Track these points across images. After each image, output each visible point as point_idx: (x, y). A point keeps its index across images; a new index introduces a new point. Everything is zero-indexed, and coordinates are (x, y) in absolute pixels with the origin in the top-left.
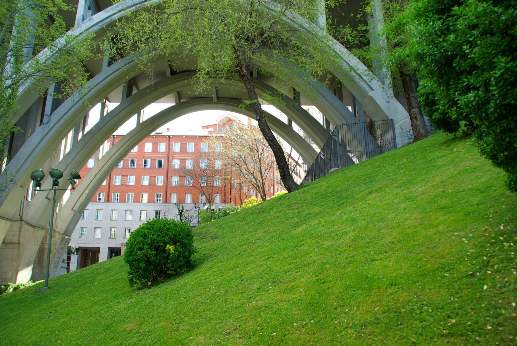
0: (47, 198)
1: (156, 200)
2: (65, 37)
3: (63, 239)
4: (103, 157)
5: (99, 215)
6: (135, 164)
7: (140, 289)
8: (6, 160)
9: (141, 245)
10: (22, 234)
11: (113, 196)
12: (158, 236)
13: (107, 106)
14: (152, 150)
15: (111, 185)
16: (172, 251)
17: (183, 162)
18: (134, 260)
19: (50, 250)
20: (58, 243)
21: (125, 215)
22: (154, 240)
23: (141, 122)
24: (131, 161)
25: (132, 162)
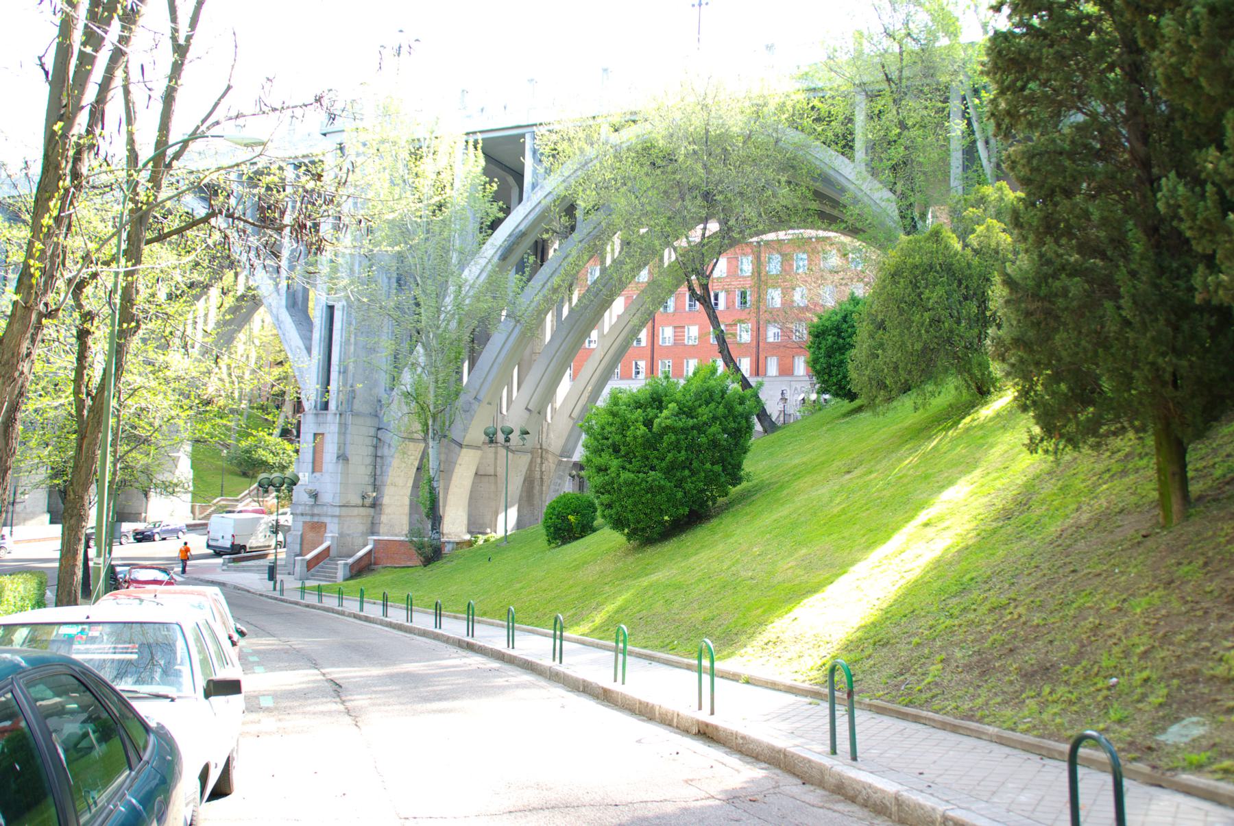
0: (527, 408)
8: (466, 365)
14: (729, 271)
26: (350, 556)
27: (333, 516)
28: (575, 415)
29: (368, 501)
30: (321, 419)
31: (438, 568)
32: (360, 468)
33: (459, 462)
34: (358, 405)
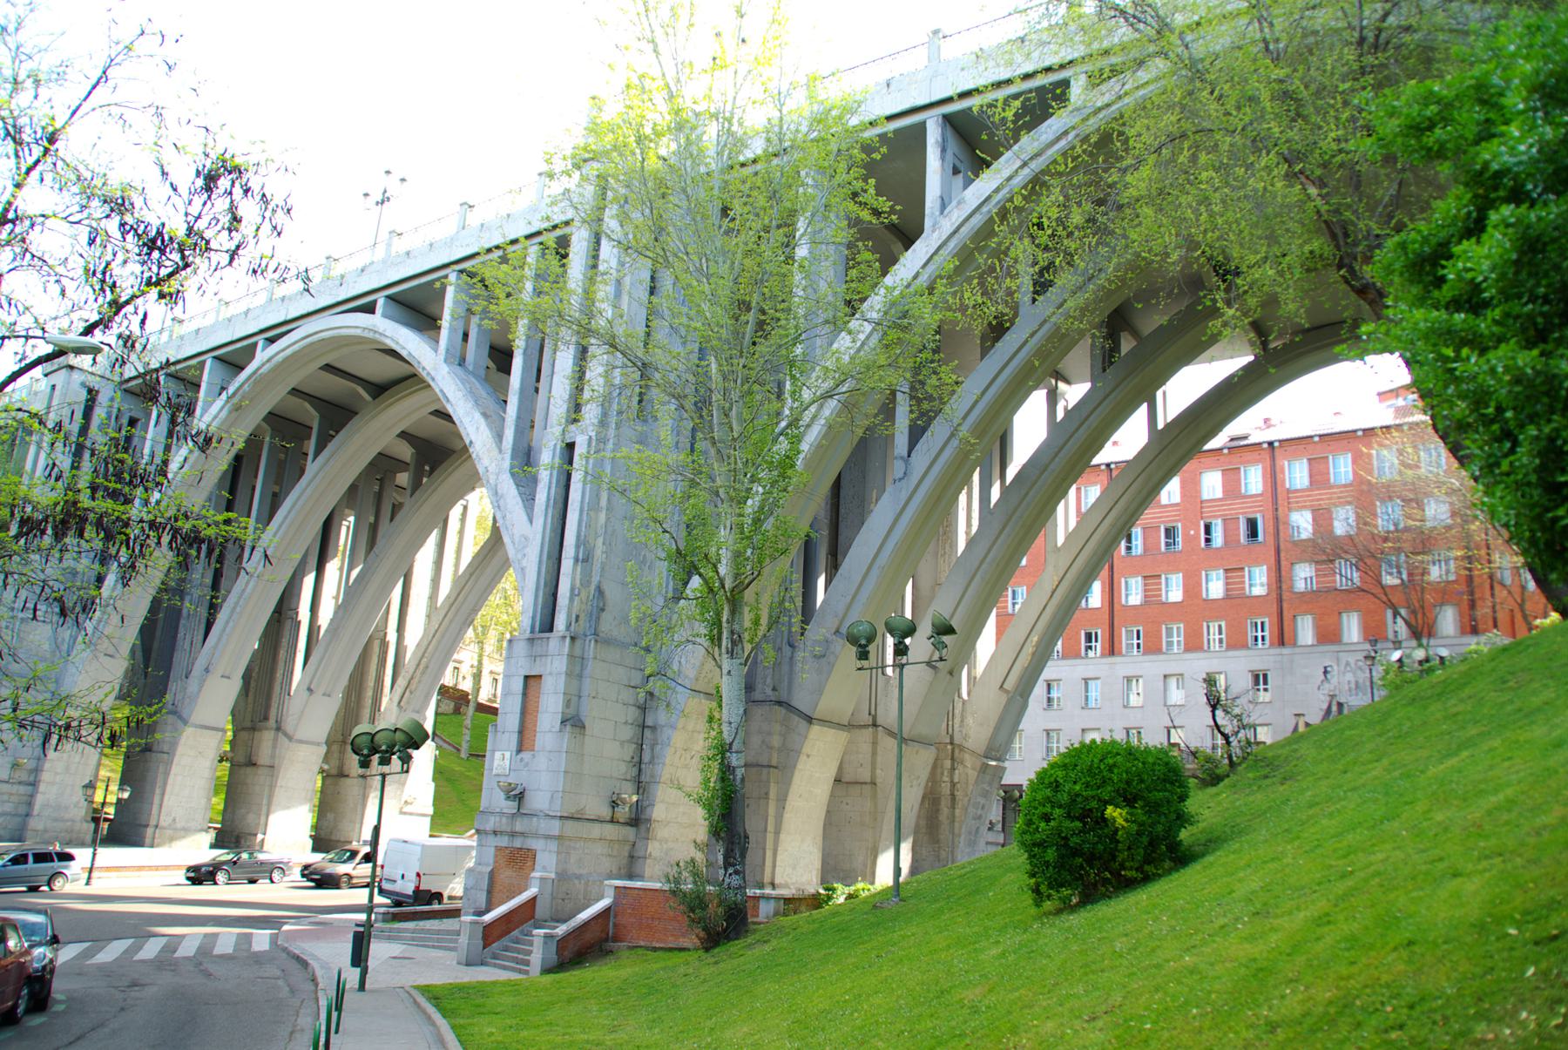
1: (1250, 641)
2: (882, 291)
4: (1069, 537)
5: (1093, 694)
6: (1179, 539)
7: (1059, 912)
9: (1048, 809)
10: (879, 759)
11: (1125, 638)
12: (1087, 785)
13: (1063, 395)
15: (1116, 606)
16: (1120, 821)
17: (1322, 518)
18: (1034, 845)
20: (972, 780)
21: (1165, 690)
22: (1077, 795)
23: (1160, 426)
24: (1167, 530)
25: (1170, 533)
27: (548, 837)
29: (623, 812)
30: (538, 649)
31: (739, 956)
32: (609, 745)
34: (608, 624)
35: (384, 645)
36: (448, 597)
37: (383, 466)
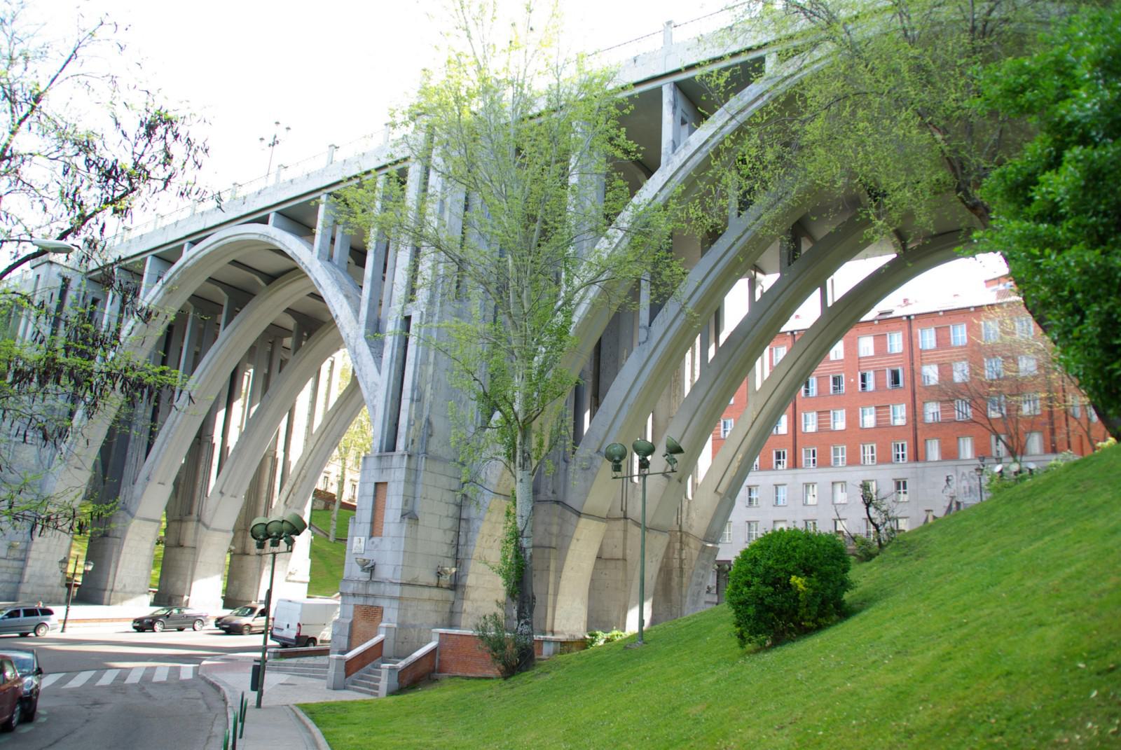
2: (631, 208)
3: (704, 547)
4: (764, 383)
6: (843, 385)
7: (757, 651)
9: (749, 578)
10: (629, 542)
11: (804, 456)
12: (777, 561)
13: (760, 282)
15: (798, 434)
16: (801, 586)
17: (945, 370)
18: (740, 603)
19: (681, 569)
21: (833, 493)
22: (770, 568)
23: (830, 304)
25: (836, 380)
26: (403, 658)
28: (722, 489)
29: (445, 580)
30: (385, 464)
31: (528, 682)
33: (576, 535)
34: (435, 446)
35: (275, 460)
36: (320, 426)
37: (273, 333)
